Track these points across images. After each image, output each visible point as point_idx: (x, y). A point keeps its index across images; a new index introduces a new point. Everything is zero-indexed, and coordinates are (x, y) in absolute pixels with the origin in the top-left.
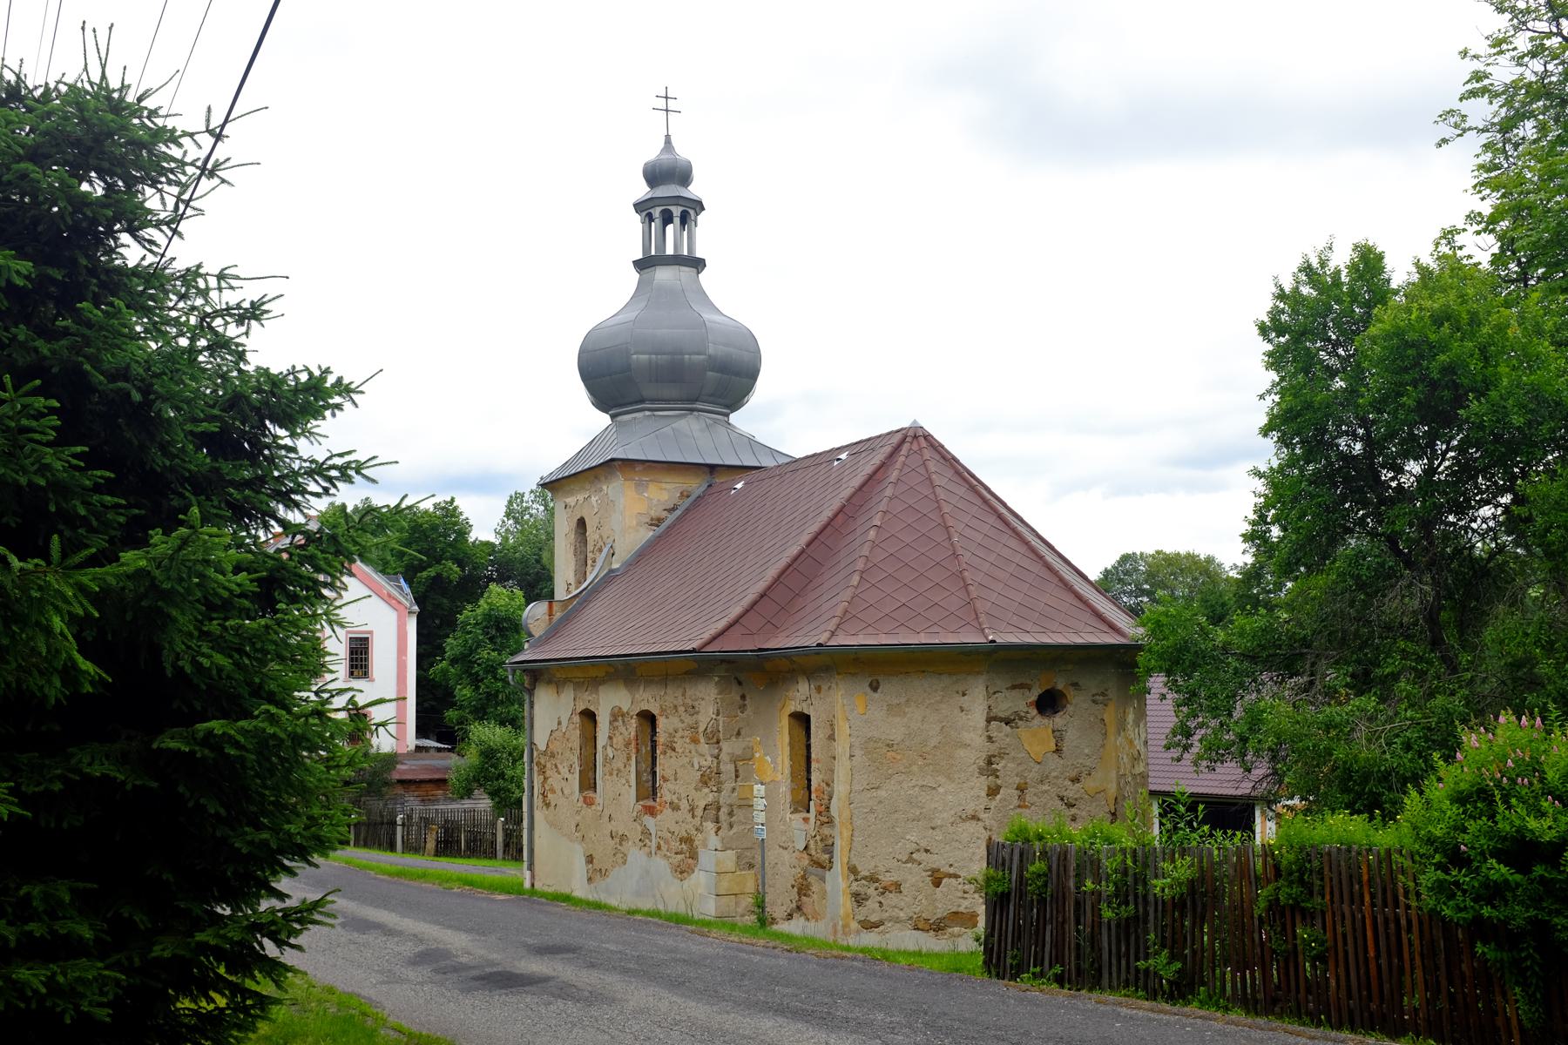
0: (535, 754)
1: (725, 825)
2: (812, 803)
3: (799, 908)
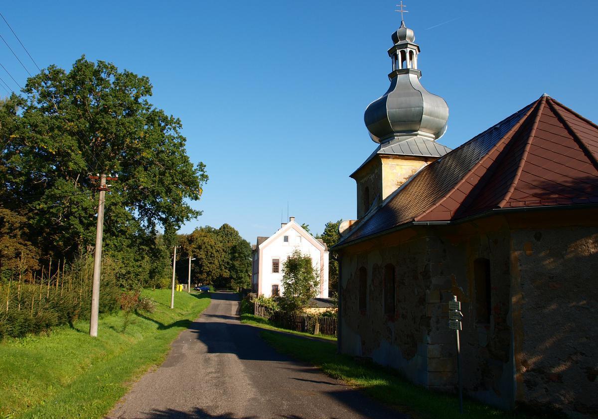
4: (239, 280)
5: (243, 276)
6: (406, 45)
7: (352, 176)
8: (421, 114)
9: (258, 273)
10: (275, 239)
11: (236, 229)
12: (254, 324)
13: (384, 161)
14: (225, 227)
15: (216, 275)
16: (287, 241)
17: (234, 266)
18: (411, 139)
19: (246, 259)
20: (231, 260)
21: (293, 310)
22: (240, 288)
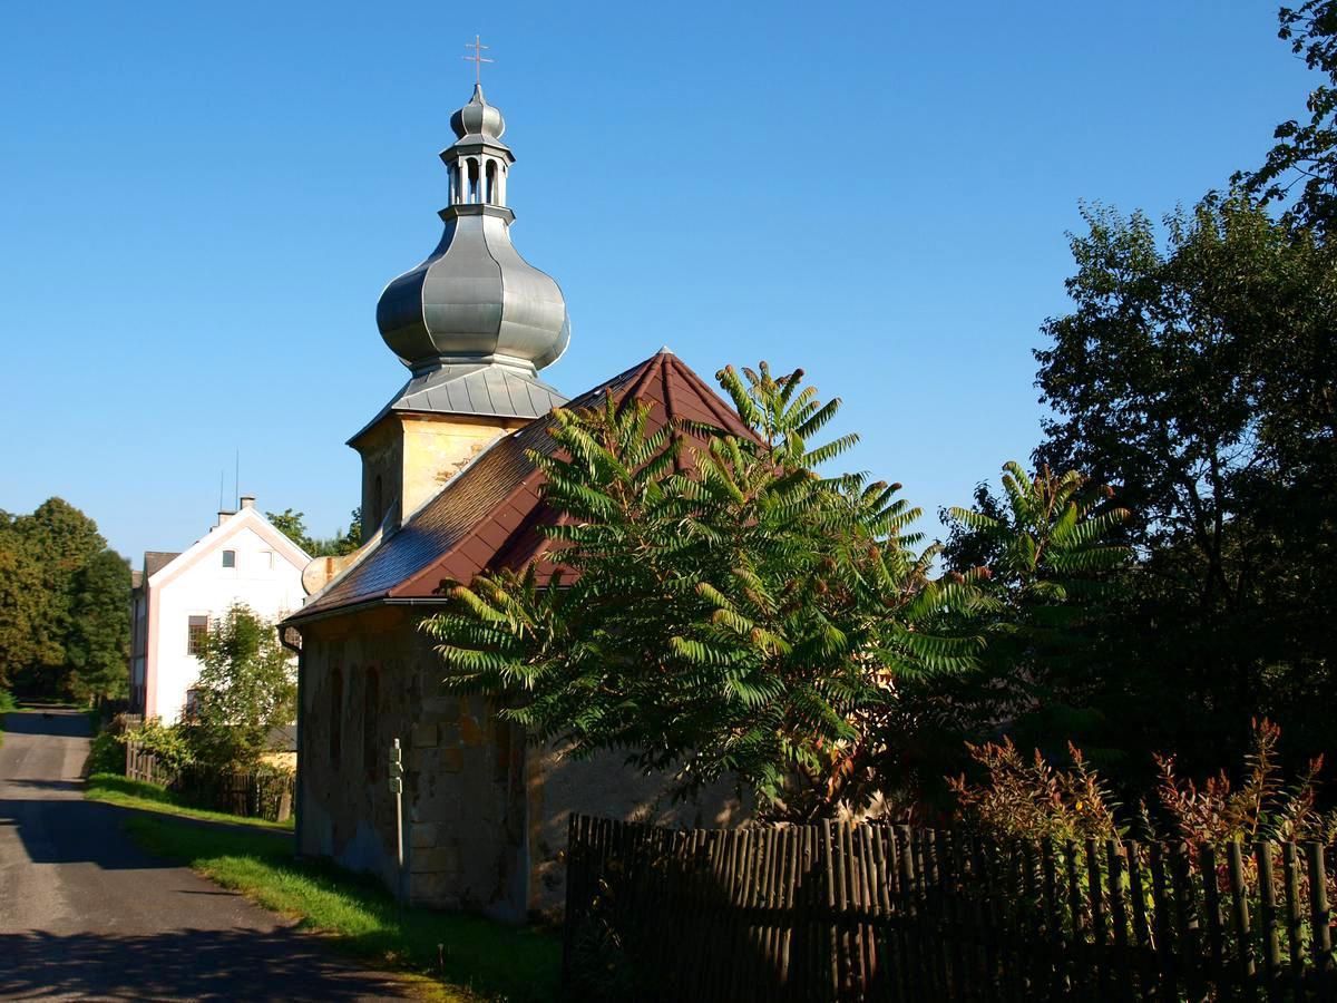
4: (94, 673)
5: (107, 658)
6: (478, 148)
7: (353, 443)
8: (497, 317)
9: (145, 656)
10: (193, 562)
11: (88, 515)
12: (119, 799)
13: (408, 426)
14: (52, 508)
15: (23, 659)
16: (233, 565)
17: (78, 629)
18: (476, 373)
19: (116, 609)
20: (70, 611)
21: (229, 760)
22: (97, 697)
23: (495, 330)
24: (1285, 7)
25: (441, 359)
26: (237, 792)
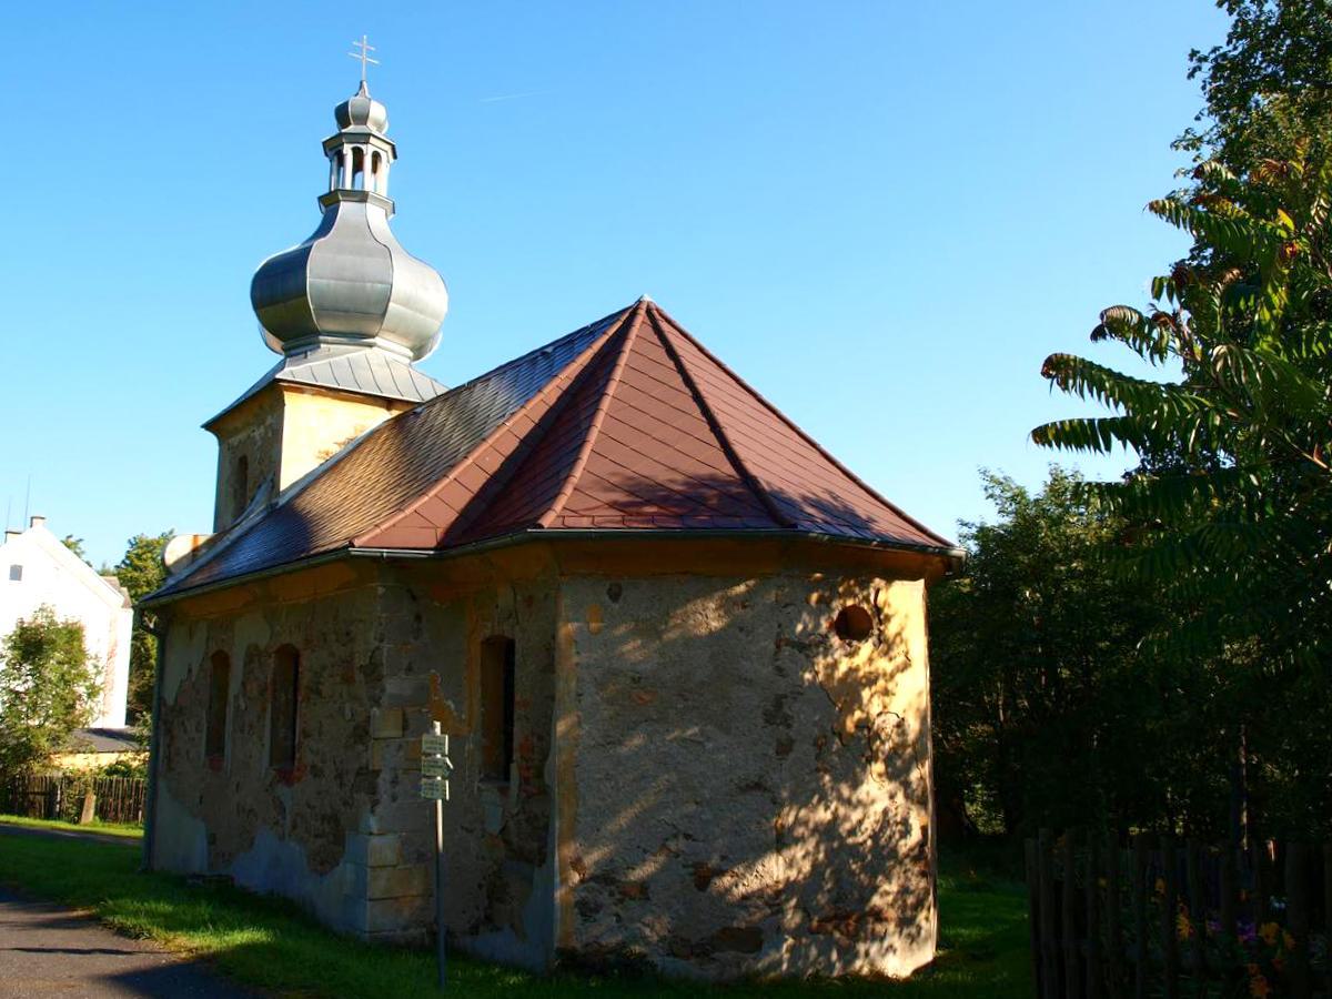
0: (163, 709)
1: (385, 798)
2: (514, 767)
3: (489, 919)
6: (366, 138)
7: (209, 426)
13: (292, 401)
16: (19, 579)
18: (357, 354)
21: (24, 760)
23: (381, 312)
24: (1196, 49)
25: (321, 338)
26: (34, 793)
